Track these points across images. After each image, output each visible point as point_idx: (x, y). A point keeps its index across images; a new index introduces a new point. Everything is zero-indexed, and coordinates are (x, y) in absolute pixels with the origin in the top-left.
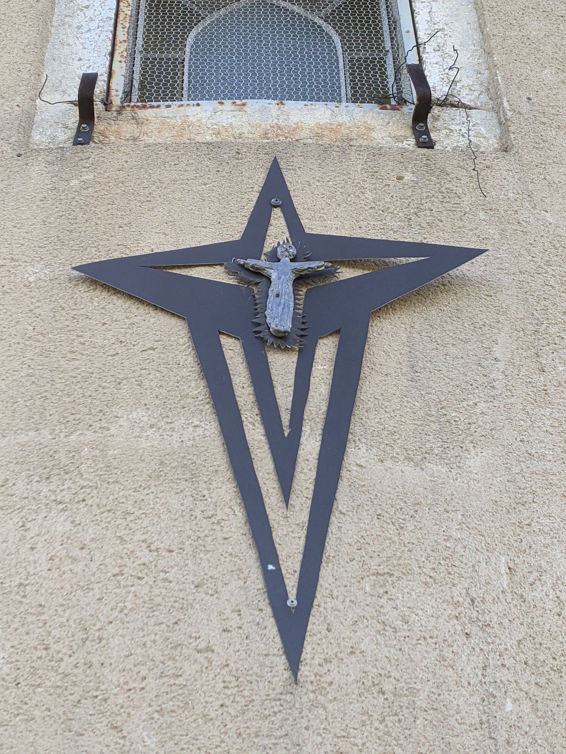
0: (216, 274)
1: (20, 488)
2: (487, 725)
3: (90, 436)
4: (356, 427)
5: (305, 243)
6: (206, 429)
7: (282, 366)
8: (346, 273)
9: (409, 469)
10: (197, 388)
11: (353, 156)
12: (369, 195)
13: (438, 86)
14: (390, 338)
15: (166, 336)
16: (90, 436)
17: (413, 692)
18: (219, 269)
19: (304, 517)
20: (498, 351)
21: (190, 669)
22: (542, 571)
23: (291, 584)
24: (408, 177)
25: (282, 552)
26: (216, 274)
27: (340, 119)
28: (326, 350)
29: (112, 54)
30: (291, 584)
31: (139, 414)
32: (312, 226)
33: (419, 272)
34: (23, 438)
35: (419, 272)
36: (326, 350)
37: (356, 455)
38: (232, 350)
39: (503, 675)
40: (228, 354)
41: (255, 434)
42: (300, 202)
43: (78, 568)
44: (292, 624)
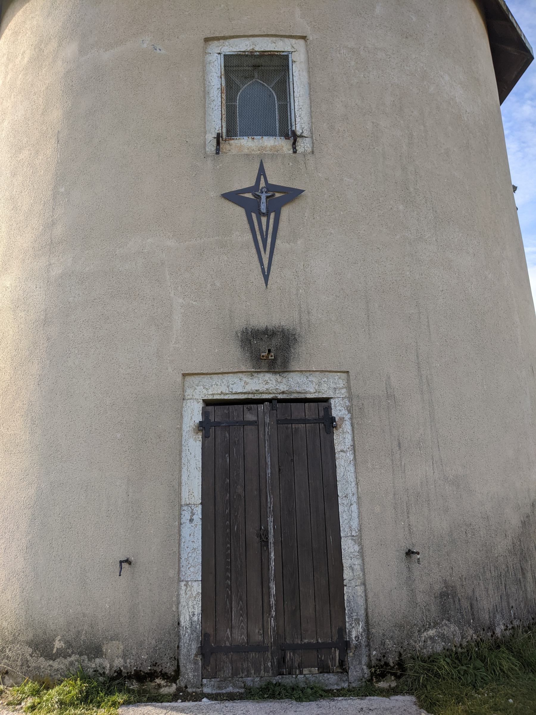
0: (249, 195)
1: (217, 250)
2: (297, 294)
3: (229, 238)
4: (278, 235)
5: (270, 188)
6: (249, 236)
7: (264, 220)
8: (277, 195)
9: (287, 245)
10: (247, 226)
11: (279, 158)
12: (282, 170)
13: (299, 132)
14: (285, 211)
15: (239, 212)
16: (229, 238)
17: (286, 289)
18: (251, 194)
19: (268, 256)
20: (306, 214)
21: (250, 286)
22: (309, 265)
23: (266, 270)
24: (291, 164)
25: (264, 264)
26: (249, 195)
27: (276, 144)
28: (272, 215)
29: (222, 119)
30: (266, 270)
31: (237, 233)
32: (270, 181)
33: (292, 195)
34: (216, 238)
35: (292, 195)
36: (272, 215)
37: (278, 242)
38: (254, 216)
39: (300, 285)
40: (253, 217)
41: (259, 237)
42: (267, 173)
43: (230, 267)
44: (266, 278)
